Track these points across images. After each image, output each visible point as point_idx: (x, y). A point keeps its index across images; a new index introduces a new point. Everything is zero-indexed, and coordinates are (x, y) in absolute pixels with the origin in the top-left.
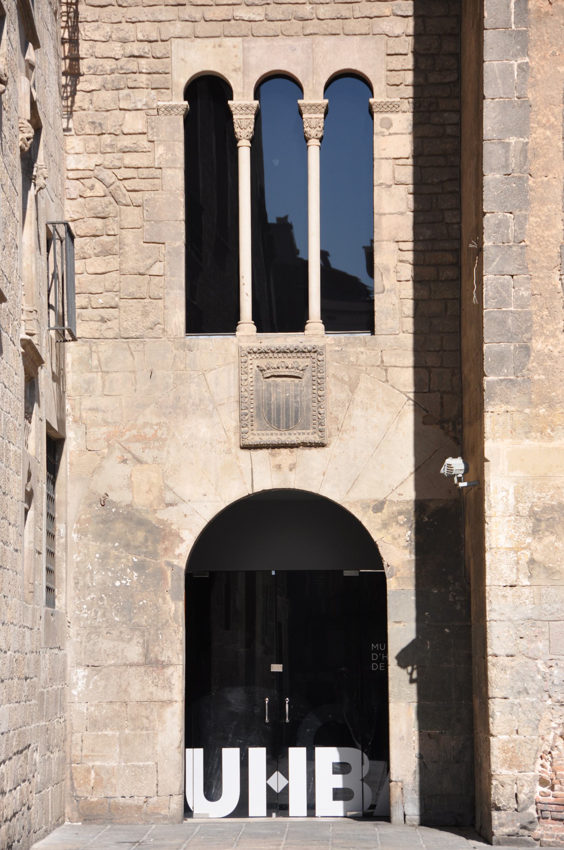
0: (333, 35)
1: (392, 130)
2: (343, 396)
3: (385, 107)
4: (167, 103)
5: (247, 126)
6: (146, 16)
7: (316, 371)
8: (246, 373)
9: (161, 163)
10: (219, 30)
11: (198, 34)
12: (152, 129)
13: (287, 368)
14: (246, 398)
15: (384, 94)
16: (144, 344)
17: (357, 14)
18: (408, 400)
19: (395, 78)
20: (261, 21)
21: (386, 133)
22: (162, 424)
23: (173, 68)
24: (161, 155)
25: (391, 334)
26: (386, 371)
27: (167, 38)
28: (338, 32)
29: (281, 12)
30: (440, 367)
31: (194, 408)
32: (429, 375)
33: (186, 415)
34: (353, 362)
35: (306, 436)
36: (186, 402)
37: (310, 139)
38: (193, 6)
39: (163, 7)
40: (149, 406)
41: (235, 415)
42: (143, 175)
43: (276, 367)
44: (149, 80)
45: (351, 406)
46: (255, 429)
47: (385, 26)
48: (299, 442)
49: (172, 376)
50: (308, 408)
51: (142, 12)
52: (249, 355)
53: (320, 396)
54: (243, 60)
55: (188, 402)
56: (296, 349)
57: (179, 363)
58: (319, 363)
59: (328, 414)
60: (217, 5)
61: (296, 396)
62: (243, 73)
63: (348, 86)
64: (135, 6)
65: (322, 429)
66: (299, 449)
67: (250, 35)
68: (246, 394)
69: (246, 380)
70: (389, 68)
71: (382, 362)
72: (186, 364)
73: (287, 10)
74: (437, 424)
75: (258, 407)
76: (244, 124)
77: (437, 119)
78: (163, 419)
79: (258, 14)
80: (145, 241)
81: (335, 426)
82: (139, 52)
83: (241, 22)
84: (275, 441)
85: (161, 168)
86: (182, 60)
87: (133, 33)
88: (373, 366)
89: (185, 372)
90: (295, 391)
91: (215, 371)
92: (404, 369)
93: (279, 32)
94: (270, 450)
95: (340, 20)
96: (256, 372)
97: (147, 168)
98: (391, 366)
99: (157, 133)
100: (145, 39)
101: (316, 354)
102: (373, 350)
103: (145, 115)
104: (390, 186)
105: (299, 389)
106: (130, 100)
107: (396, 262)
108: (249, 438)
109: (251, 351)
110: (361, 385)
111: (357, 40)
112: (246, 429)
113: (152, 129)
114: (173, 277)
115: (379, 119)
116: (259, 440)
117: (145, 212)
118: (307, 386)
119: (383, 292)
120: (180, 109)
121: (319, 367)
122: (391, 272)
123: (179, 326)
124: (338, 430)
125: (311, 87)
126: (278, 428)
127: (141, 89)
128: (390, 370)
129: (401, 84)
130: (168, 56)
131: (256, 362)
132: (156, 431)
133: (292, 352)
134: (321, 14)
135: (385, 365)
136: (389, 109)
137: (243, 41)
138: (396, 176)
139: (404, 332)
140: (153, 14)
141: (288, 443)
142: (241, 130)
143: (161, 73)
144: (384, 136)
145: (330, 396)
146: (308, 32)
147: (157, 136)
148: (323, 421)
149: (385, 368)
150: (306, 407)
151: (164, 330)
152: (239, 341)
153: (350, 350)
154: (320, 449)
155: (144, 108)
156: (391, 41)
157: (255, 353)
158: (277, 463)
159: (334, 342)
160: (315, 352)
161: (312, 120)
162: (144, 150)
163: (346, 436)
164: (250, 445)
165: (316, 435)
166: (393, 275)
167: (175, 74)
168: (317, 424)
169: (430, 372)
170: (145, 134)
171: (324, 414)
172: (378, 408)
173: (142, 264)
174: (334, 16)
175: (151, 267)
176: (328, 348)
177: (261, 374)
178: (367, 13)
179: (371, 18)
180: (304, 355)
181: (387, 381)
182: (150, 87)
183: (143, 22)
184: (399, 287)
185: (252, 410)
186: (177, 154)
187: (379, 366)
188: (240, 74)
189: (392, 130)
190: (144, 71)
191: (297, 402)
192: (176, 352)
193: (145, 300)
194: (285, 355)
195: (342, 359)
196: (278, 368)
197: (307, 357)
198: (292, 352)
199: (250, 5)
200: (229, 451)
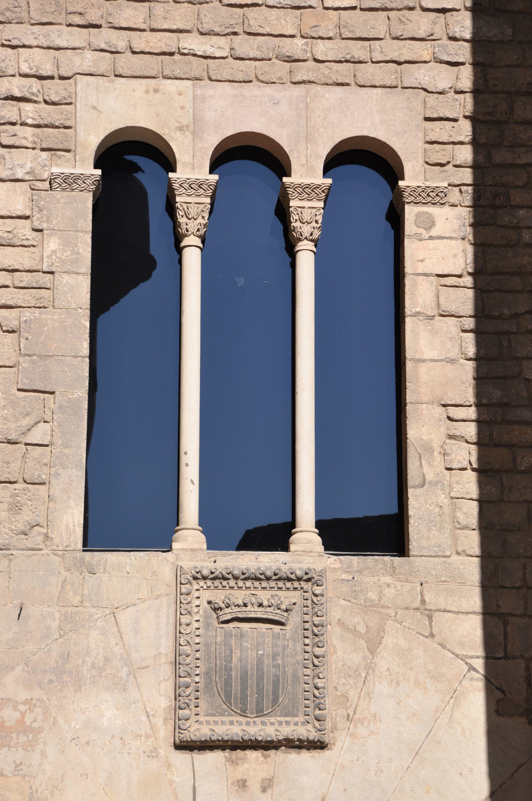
0: (338, 84)
1: (434, 232)
2: (356, 659)
3: (424, 195)
4: (67, 170)
5: (198, 214)
6: (36, 38)
7: (310, 613)
8: (189, 613)
9: (53, 264)
10: (155, 67)
11: (120, 71)
12: (41, 210)
13: (260, 605)
14: (188, 656)
15: (422, 177)
16: (10, 560)
17: (378, 57)
18: (469, 671)
19: (439, 154)
20: (224, 58)
21: (425, 235)
22: (34, 701)
23: (78, 120)
24: (54, 252)
25: (438, 556)
26: (430, 617)
27: (70, 74)
28: (347, 81)
29: (255, 47)
30: (522, 616)
31: (94, 672)
32: (505, 629)
33: (80, 686)
34: (372, 600)
35: (292, 727)
36: (80, 661)
37: (300, 240)
38: (113, 30)
39: (64, 27)
40: (13, 669)
41: (168, 687)
42: (21, 281)
43: (241, 603)
44: (37, 136)
45: (371, 677)
46: (202, 713)
47: (421, 75)
48: (281, 738)
49: (57, 615)
50: (296, 678)
51: (29, 32)
52: (194, 582)
53: (317, 657)
54: (194, 114)
55: (83, 662)
56: (275, 574)
57: (71, 594)
58: (315, 599)
59: (330, 689)
60: (153, 30)
61: (275, 656)
62: (193, 133)
63: (364, 161)
64: (17, 23)
65: (322, 715)
66: (278, 752)
67: (206, 78)
68: (187, 649)
69: (188, 625)
70: (428, 139)
71: (423, 601)
72: (83, 595)
73: (266, 45)
74: (522, 715)
75: (207, 674)
76: (193, 211)
77: (507, 219)
78: (38, 693)
79: (219, 48)
80: (20, 387)
81: (342, 712)
82: (21, 91)
83: (191, 57)
84: (237, 734)
85: (52, 273)
86: (94, 108)
87: (12, 63)
88: (407, 608)
89: (80, 609)
90: (274, 646)
91: (133, 609)
92: (460, 616)
93: (252, 77)
94: (227, 753)
95: (349, 64)
96: (205, 611)
97: (29, 271)
98: (438, 610)
99: (48, 218)
100: (33, 72)
101: (310, 584)
102: (407, 581)
103: (29, 189)
104: (432, 318)
105: (280, 643)
106: (5, 165)
107: (444, 438)
108: (192, 729)
109: (199, 576)
110: (388, 641)
111: (377, 94)
112: (186, 712)
113: (41, 210)
114: (66, 447)
115: (413, 214)
116: (209, 733)
117: (22, 340)
118: (293, 638)
119: (423, 485)
120: (88, 182)
121: (315, 605)
122: (436, 453)
123: (74, 530)
124: (348, 719)
125: (303, 161)
126: (243, 713)
127: (24, 149)
128: (436, 616)
129: (448, 163)
130: (70, 101)
131: (206, 595)
132: (23, 715)
133: (268, 579)
134: (319, 52)
135: (428, 608)
136: (430, 199)
137: (194, 85)
138: (442, 301)
139: (458, 553)
140: (46, 36)
141: (260, 739)
142: (188, 221)
143: (57, 127)
144: (421, 240)
145: (334, 658)
146: (298, 78)
147: (48, 222)
148: (322, 701)
149: (428, 612)
150: (293, 676)
151: (47, 537)
152: (178, 557)
153: (370, 580)
154: (316, 753)
155: (27, 177)
156: (432, 99)
157: (205, 578)
158: (240, 777)
159: (339, 565)
160: (308, 580)
161: (305, 210)
162: (26, 243)
163: (361, 730)
164: (192, 741)
165: (310, 727)
166: (438, 458)
167: (81, 129)
168: (312, 706)
169: (506, 624)
170: (27, 218)
171: (324, 688)
172: (417, 682)
173: (13, 426)
174: (340, 57)
175: (29, 430)
176: (330, 576)
177: (215, 616)
178: (394, 56)
179: (399, 63)
180: (289, 584)
181: (432, 635)
182: (39, 147)
183: (30, 47)
184: (448, 478)
185: (197, 679)
186: (81, 251)
187: (417, 609)
188: (189, 136)
189: (434, 232)
190: (30, 121)
191: (277, 666)
192: (66, 574)
193: (16, 486)
194: (257, 584)
195: (354, 595)
196: (245, 605)
197: (295, 589)
198: (268, 579)
199: (205, 34)
200: (153, 754)
